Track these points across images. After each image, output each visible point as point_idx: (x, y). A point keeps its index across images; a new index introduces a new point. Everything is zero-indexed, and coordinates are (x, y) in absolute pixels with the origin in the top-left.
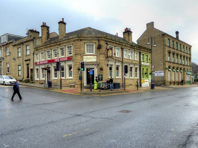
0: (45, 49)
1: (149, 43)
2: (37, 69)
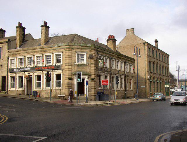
0: (25, 55)
1: (135, 54)
2: (13, 78)
